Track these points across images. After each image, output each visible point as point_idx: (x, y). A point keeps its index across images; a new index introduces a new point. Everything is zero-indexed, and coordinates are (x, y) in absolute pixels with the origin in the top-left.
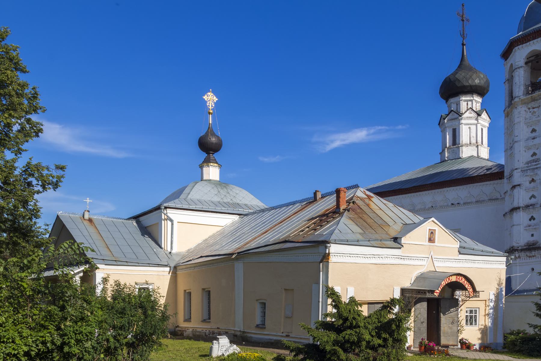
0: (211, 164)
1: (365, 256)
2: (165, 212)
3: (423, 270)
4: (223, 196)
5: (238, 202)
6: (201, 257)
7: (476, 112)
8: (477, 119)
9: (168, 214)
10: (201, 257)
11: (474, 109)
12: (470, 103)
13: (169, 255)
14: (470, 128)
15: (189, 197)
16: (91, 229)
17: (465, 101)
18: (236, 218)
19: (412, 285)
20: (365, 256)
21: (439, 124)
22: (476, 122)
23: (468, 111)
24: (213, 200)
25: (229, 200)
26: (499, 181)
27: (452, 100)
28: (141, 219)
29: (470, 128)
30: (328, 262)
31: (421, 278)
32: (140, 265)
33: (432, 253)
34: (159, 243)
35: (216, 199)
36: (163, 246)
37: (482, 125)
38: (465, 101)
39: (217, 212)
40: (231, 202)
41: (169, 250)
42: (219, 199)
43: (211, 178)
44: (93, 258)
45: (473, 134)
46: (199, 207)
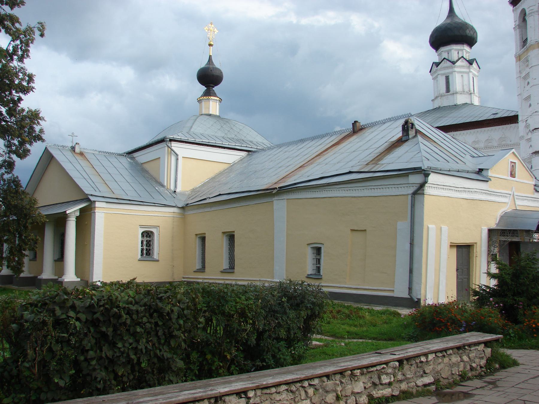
0: (212, 97)
1: (457, 189)
2: (169, 145)
3: (508, 208)
4: (226, 132)
5: (243, 138)
6: (350, 172)
7: (467, 61)
8: (469, 68)
9: (173, 148)
10: (350, 172)
11: (465, 57)
12: (460, 52)
13: (174, 195)
14: (462, 76)
15: (192, 130)
16: (83, 163)
17: (456, 50)
18: (244, 154)
19: (497, 225)
20: (457, 189)
21: (430, 72)
22: (467, 70)
23: (460, 60)
24: (216, 135)
25: (233, 136)
26: (513, 125)
27: (443, 49)
28: (135, 155)
29: (462, 76)
30: (424, 194)
31: (505, 217)
32: (145, 204)
33: (514, 190)
34: (161, 181)
35: (220, 134)
36: (165, 184)
37: (474, 74)
38: (456, 50)
39: (224, 148)
40: (236, 138)
41: (172, 188)
42: (223, 135)
43: (210, 113)
44: (91, 195)
45: (466, 83)
46: (205, 141)
